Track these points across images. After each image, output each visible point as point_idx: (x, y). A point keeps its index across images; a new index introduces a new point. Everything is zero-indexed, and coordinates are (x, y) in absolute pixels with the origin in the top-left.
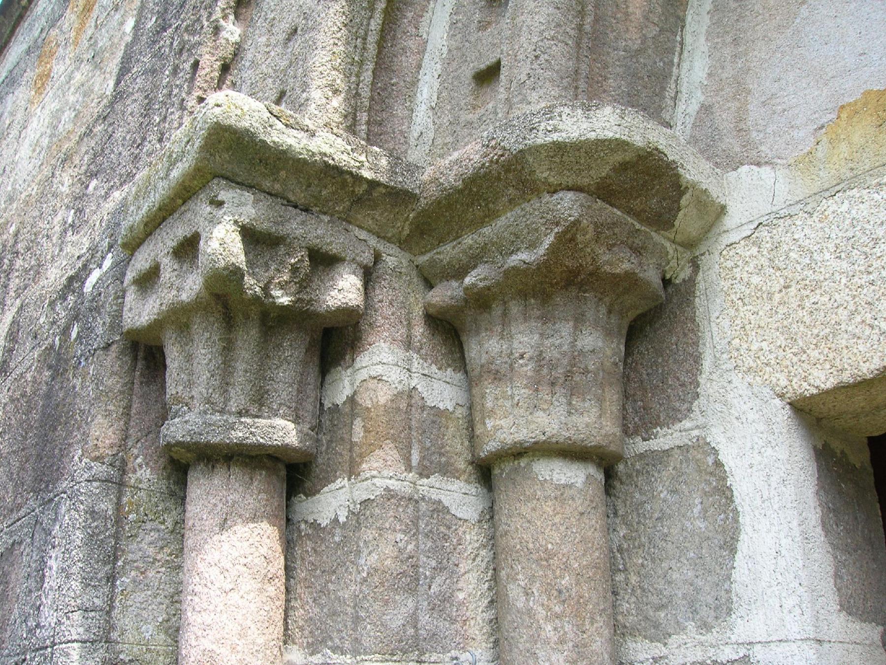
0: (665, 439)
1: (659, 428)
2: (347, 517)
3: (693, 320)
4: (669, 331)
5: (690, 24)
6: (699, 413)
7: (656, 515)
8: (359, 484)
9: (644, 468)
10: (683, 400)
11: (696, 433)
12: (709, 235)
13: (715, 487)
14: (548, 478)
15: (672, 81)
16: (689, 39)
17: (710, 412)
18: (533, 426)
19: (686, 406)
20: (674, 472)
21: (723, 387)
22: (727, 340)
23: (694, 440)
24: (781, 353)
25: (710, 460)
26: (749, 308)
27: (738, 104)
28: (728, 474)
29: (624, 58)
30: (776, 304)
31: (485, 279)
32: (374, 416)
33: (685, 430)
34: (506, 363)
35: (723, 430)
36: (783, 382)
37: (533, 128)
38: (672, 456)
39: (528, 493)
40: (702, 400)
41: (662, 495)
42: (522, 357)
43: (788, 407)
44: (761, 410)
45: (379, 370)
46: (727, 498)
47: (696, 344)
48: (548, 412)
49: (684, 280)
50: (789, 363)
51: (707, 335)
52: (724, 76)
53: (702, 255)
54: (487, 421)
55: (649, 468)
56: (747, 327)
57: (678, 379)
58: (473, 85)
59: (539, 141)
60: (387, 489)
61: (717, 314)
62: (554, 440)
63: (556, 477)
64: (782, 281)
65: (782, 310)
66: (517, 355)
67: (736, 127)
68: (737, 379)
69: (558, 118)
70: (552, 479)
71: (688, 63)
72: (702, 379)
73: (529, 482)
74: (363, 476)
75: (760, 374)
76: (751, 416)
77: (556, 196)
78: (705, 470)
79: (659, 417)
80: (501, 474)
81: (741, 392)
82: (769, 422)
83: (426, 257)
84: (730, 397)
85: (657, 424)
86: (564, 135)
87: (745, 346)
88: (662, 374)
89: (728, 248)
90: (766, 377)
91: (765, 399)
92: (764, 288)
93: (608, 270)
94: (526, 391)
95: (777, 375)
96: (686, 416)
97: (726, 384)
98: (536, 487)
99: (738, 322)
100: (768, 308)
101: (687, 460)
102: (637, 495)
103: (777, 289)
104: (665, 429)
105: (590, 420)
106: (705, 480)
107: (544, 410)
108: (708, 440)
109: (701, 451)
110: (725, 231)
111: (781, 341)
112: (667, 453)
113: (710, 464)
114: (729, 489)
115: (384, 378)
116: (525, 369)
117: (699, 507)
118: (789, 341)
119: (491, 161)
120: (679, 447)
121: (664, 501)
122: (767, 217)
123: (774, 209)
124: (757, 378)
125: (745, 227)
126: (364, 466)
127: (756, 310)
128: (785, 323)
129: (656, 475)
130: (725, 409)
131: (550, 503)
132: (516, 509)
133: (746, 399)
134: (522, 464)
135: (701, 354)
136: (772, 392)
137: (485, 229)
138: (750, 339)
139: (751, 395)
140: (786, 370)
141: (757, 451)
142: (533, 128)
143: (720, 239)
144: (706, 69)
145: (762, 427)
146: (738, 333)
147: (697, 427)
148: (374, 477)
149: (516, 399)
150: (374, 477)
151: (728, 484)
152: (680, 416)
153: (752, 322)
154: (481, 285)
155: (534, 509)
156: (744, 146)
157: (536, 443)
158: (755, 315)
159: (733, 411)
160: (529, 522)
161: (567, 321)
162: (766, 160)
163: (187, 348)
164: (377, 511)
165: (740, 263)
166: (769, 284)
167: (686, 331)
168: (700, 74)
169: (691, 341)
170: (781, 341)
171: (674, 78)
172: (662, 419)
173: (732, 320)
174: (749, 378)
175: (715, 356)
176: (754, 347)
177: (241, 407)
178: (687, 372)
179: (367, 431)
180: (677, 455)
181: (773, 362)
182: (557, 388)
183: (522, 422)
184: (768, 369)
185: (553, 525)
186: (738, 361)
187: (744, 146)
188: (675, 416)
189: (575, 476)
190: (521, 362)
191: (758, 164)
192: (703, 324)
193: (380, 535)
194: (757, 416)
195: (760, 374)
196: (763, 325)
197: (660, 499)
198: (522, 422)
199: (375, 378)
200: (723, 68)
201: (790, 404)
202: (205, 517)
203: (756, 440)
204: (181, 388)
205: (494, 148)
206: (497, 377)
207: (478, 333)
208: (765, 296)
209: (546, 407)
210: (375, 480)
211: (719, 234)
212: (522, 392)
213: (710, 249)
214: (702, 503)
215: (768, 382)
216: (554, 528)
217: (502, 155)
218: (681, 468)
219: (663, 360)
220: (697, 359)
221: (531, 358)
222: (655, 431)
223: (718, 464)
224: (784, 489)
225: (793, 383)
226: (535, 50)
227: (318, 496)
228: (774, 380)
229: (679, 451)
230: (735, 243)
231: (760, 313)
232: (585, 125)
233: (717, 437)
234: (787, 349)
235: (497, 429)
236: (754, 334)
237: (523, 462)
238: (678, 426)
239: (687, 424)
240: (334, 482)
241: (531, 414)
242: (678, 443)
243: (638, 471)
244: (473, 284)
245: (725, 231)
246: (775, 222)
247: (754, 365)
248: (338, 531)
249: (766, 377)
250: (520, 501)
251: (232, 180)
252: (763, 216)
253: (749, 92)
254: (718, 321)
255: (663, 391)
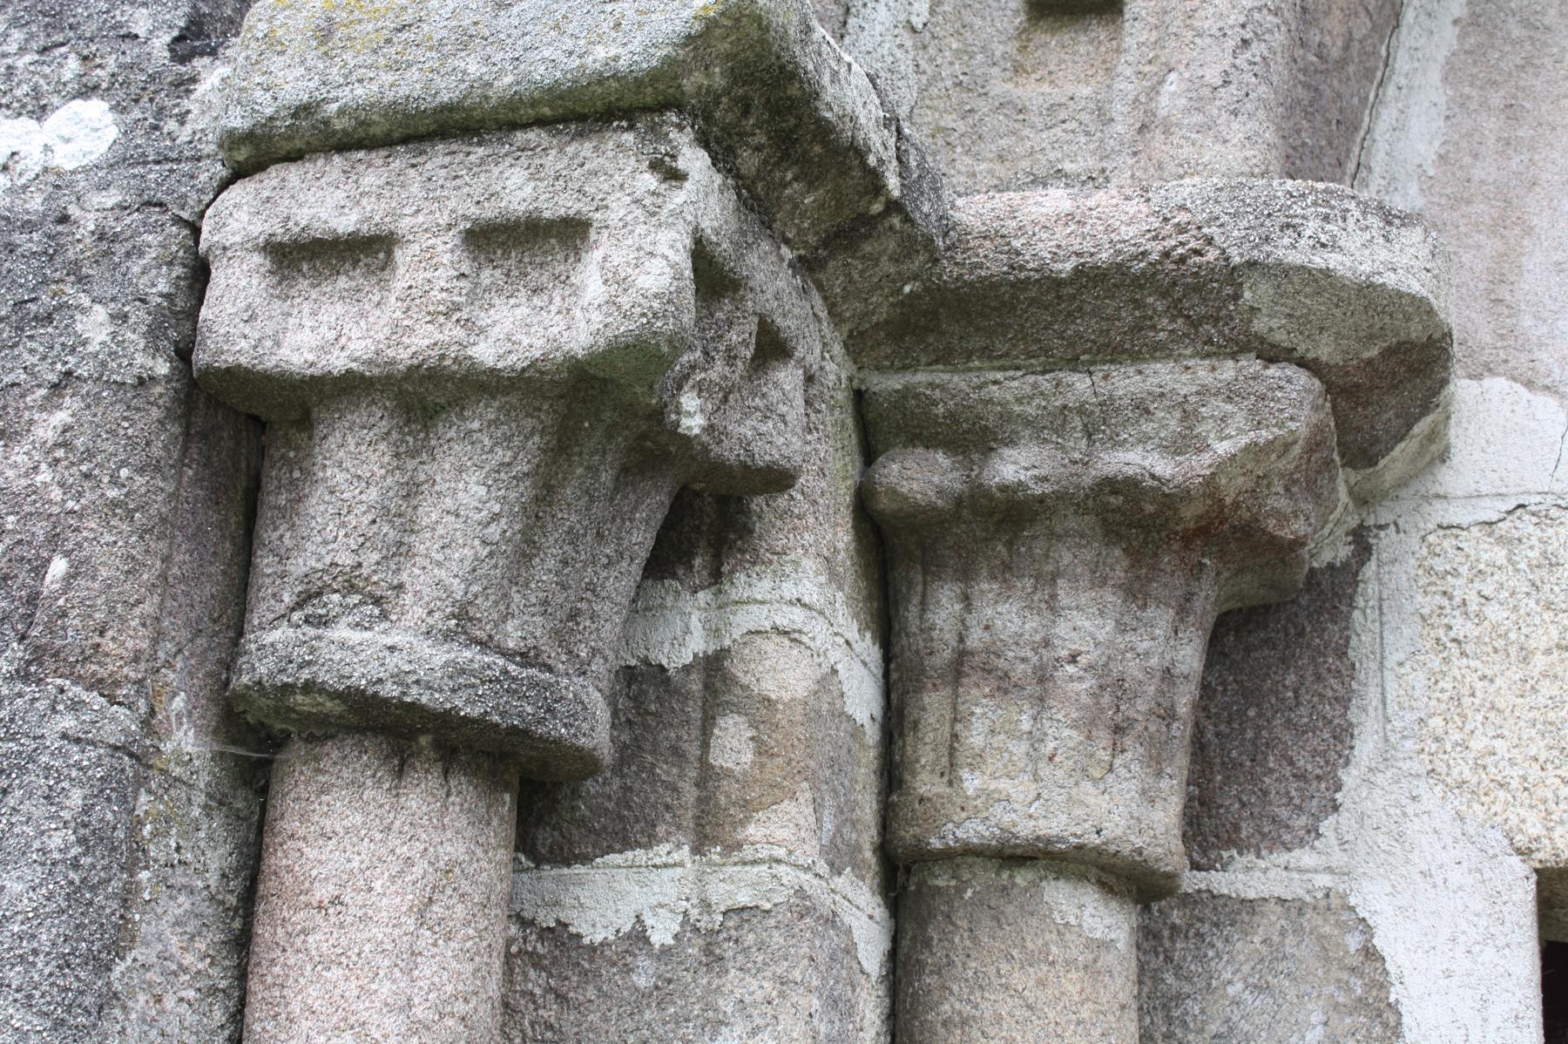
0: (1245, 877)
1: (1234, 852)
2: (676, 937)
3: (1342, 654)
4: (1283, 660)
5: (1410, 28)
6: (1333, 841)
7: (1213, 1028)
8: (730, 870)
9: (1190, 926)
10: (1299, 808)
11: (1323, 880)
12: (1403, 493)
13: (1360, 1000)
14: (1073, 921)
15: (1358, 140)
16: (1402, 62)
17: (1361, 848)
18: (1079, 812)
19: (1303, 820)
20: (1264, 950)
21: (1398, 805)
22: (1416, 715)
23: (1320, 895)
24: (1534, 772)
25: (1353, 942)
26: (1472, 664)
27: (1499, 244)
28: (1392, 978)
29: (1316, 71)
30: (1536, 674)
31: (1045, 479)
32: (784, 723)
33: (1300, 870)
34: (1024, 660)
35: (1389, 889)
36: (1534, 828)
37: (1288, 226)
38: (1263, 914)
39: (1029, 945)
40: (1345, 819)
41: (1231, 990)
42: (1073, 659)
43: (1534, 877)
44: (1480, 871)
45: (793, 617)
46: (1386, 1025)
47: (1344, 702)
48: (1102, 787)
49: (1331, 566)
50: (1550, 795)
51: (1373, 694)
52: (1478, 174)
53: (1381, 527)
54: (965, 774)
55: (1205, 928)
56: (1467, 701)
57: (1291, 763)
58: (1023, 17)
59: (1294, 258)
60: (800, 892)
61: (1401, 656)
62: (1113, 848)
63: (1088, 922)
64: (1554, 633)
65: (1547, 689)
66: (1064, 653)
67: (1490, 292)
68: (1431, 796)
69: (1340, 222)
70: (1080, 926)
71: (1395, 113)
72: (1350, 777)
73: (1034, 922)
74: (748, 852)
75: (1483, 799)
76: (1456, 876)
77: (1273, 371)
78: (1340, 960)
79: (1237, 828)
80: (960, 891)
81: (1438, 825)
82: (1494, 898)
83: (895, 382)
84: (1413, 827)
85: (1231, 843)
86: (1348, 261)
87: (1456, 736)
88: (1253, 742)
89: (1441, 532)
90: (1497, 808)
91: (1491, 852)
92: (1513, 636)
93: (1270, 528)
94: (1074, 733)
95: (1522, 812)
96: (1302, 843)
97: (1404, 801)
98: (1048, 936)
99: (1446, 684)
100: (1517, 677)
101: (1300, 931)
102: (1170, 978)
103: (1543, 646)
104: (1252, 857)
105: (1132, 808)
106: (1339, 981)
107: (1095, 781)
108: (1352, 901)
109: (1332, 919)
110: (1438, 496)
111: (1538, 748)
112: (1250, 906)
113: (1352, 950)
114: (1394, 1008)
115: (805, 639)
116: (1077, 686)
117: (1320, 1029)
118: (1556, 753)
119: (1166, 254)
120: (1281, 901)
121: (1236, 1003)
122: (1539, 498)
123: (1557, 488)
124: (1476, 806)
125: (1487, 502)
126: (752, 830)
127: (1489, 673)
128: (1552, 716)
129: (1219, 945)
130: (1398, 849)
131: (1073, 975)
132: (1000, 976)
133: (1449, 841)
134: (1019, 880)
135: (1351, 725)
136: (1506, 842)
137: (1076, 377)
138: (1469, 727)
139: (1459, 836)
140: (1542, 807)
141: (1463, 948)
142: (1288, 226)
143: (1426, 508)
144: (1437, 144)
145: (1478, 904)
146: (1444, 706)
147: (1329, 870)
148: (778, 861)
149: (1051, 745)
150: (778, 861)
151: (1392, 999)
152: (1287, 837)
153: (1478, 693)
154: (1038, 490)
155: (1041, 983)
156: (1502, 337)
157: (1079, 847)
158: (1486, 683)
159: (1414, 857)
160: (1029, 1007)
161: (1167, 605)
162: (1547, 382)
163: (411, 464)
164: (777, 938)
165: (1464, 570)
166: (1525, 630)
167: (1323, 671)
168: (1422, 148)
169: (1330, 694)
170: (1538, 748)
171: (1362, 133)
172: (1244, 834)
173: (1434, 679)
174: (1459, 801)
175: (1386, 740)
176: (1478, 744)
177: (531, 642)
178: (1315, 753)
179: (762, 749)
180: (1273, 919)
181: (1515, 784)
182: (1128, 741)
183: (1059, 797)
184: (1502, 794)
185: (1079, 1023)
186: (1437, 763)
187: (1502, 337)
188: (1274, 837)
189: (1100, 920)
190: (1070, 669)
191: (1529, 384)
192: (1367, 669)
193: (782, 995)
194: (1470, 880)
195: (1483, 799)
196: (1501, 706)
197: (1224, 996)
198: (1059, 797)
199: (786, 633)
200: (1476, 156)
201: (1537, 871)
202: (377, 885)
203: (1464, 926)
204: (376, 556)
205: (1181, 229)
206: (1004, 685)
207: (966, 575)
208: (1513, 651)
209: (1097, 774)
210: (781, 869)
211: (1426, 498)
212: (1062, 734)
213: (1401, 522)
214: (1326, 1024)
215: (1498, 819)
216: (1080, 1028)
217: (1197, 252)
218: (1282, 943)
219: (1260, 715)
220: (1343, 734)
221: (1090, 667)
222: (1225, 854)
223: (1370, 953)
224: (1516, 1032)
225: (1556, 835)
226: (1243, 26)
227: (579, 869)
228: (1514, 821)
229: (1278, 909)
230: (1459, 527)
231: (1498, 681)
232: (1383, 255)
233: (1373, 899)
234: (1549, 766)
235: (991, 797)
236: (1479, 718)
237: (1022, 878)
238: (1282, 858)
239: (1306, 857)
240: (648, 846)
241: (1077, 784)
242: (1280, 891)
243: (1174, 928)
244: (1020, 483)
245: (1438, 496)
246: (1554, 512)
247: (1475, 780)
248: (643, 962)
249: (1497, 808)
250: (1009, 958)
251: (722, 153)
252: (1529, 493)
253: (1529, 231)
254: (1402, 671)
255: (1253, 778)
